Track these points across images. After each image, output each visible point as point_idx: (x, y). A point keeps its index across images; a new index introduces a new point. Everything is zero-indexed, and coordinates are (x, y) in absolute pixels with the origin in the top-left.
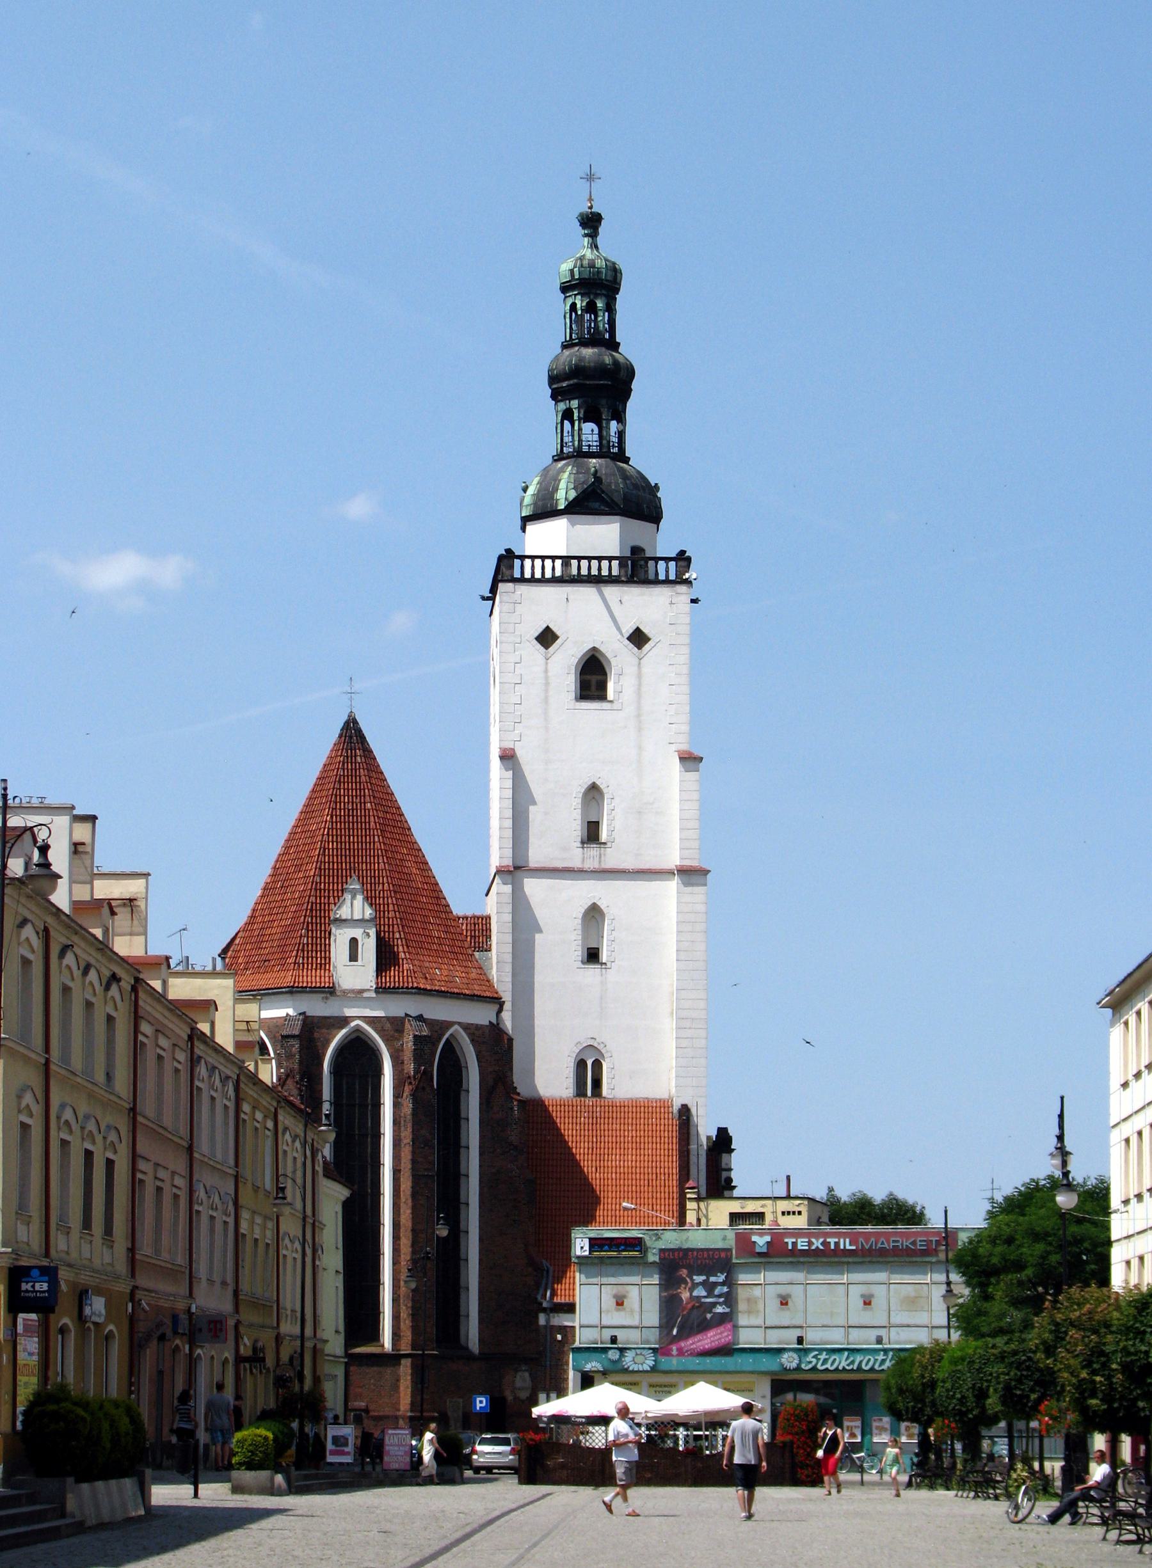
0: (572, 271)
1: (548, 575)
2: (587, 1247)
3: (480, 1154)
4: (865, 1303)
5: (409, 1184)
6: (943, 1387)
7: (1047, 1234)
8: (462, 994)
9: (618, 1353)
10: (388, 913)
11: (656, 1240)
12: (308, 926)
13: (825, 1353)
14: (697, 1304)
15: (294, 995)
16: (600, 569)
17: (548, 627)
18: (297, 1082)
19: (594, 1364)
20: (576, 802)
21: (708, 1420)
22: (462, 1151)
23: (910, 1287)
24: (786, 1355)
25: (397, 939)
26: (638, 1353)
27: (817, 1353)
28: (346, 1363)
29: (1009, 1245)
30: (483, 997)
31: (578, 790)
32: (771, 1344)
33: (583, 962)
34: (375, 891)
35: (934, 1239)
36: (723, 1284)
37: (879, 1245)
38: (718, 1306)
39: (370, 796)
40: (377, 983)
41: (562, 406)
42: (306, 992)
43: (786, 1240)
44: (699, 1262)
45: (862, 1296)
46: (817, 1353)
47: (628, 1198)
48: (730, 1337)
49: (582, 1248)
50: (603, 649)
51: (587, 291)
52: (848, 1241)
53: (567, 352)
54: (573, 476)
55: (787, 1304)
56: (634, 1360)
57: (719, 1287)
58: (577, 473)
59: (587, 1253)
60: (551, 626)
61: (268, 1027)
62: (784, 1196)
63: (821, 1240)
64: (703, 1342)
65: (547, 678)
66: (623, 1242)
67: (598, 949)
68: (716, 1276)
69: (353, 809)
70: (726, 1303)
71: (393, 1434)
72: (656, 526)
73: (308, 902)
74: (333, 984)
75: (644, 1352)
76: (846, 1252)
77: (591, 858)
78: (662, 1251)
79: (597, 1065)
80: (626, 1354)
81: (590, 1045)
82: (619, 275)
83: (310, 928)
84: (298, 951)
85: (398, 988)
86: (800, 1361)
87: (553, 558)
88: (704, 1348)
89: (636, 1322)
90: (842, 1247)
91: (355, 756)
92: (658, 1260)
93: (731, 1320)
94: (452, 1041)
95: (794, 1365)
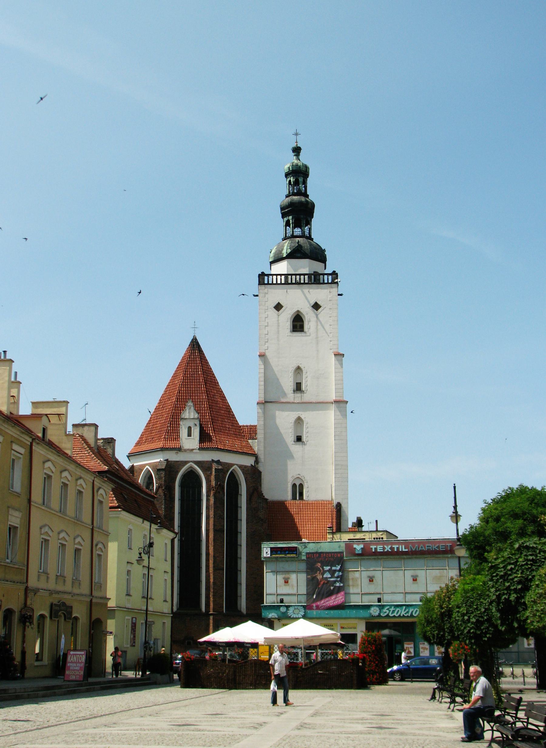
0: (289, 168)
1: (279, 282)
2: (269, 552)
3: (246, 523)
4: (414, 580)
5: (213, 535)
6: (458, 612)
7: (524, 513)
8: (238, 451)
9: (285, 608)
10: (206, 417)
11: (304, 548)
12: (171, 422)
13: (393, 607)
14: (326, 582)
15: (163, 451)
16: (300, 279)
17: (279, 303)
18: (163, 490)
19: (273, 614)
20: (291, 374)
21: (306, 644)
22: (239, 522)
23: (438, 571)
24: (372, 609)
25: (209, 427)
26: (296, 608)
27: (389, 607)
28: (172, 617)
29: (497, 522)
30: (248, 453)
31: (292, 368)
32: (365, 603)
33: (294, 442)
34: (201, 407)
35: (449, 545)
36: (339, 571)
37: (420, 549)
38: (337, 582)
39: (200, 369)
40: (200, 446)
41: (286, 219)
42: (168, 450)
43: (371, 547)
44: (327, 559)
45: (412, 576)
46: (389, 607)
47: (307, 538)
48: (343, 599)
49: (267, 553)
50: (302, 311)
51: (295, 175)
52: (403, 546)
53: (287, 199)
54: (289, 244)
55: (372, 581)
56: (293, 612)
57: (337, 573)
58: (291, 243)
59: (269, 555)
60: (280, 302)
61: (153, 467)
62: (375, 530)
63: (390, 546)
64: (329, 602)
65: (278, 323)
66: (288, 549)
67: (301, 436)
68: (336, 566)
69: (193, 374)
70: (341, 581)
71: (74, 654)
72: (324, 264)
73: (172, 413)
74: (180, 446)
75: (299, 608)
76: (403, 553)
77: (298, 397)
78: (307, 553)
79: (301, 486)
80: (289, 609)
81: (298, 477)
82: (308, 169)
83: (172, 423)
84: (166, 433)
85: (209, 448)
86: (380, 612)
87: (281, 275)
88: (330, 606)
89: (294, 592)
90: (400, 550)
91: (195, 353)
92: (305, 559)
93: (344, 590)
94: (234, 472)
95: (377, 614)
